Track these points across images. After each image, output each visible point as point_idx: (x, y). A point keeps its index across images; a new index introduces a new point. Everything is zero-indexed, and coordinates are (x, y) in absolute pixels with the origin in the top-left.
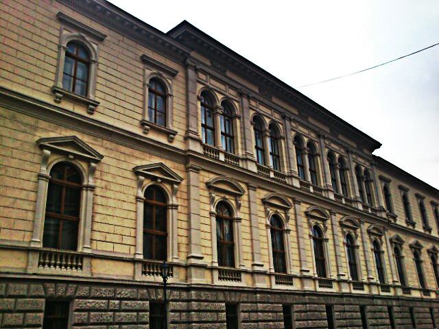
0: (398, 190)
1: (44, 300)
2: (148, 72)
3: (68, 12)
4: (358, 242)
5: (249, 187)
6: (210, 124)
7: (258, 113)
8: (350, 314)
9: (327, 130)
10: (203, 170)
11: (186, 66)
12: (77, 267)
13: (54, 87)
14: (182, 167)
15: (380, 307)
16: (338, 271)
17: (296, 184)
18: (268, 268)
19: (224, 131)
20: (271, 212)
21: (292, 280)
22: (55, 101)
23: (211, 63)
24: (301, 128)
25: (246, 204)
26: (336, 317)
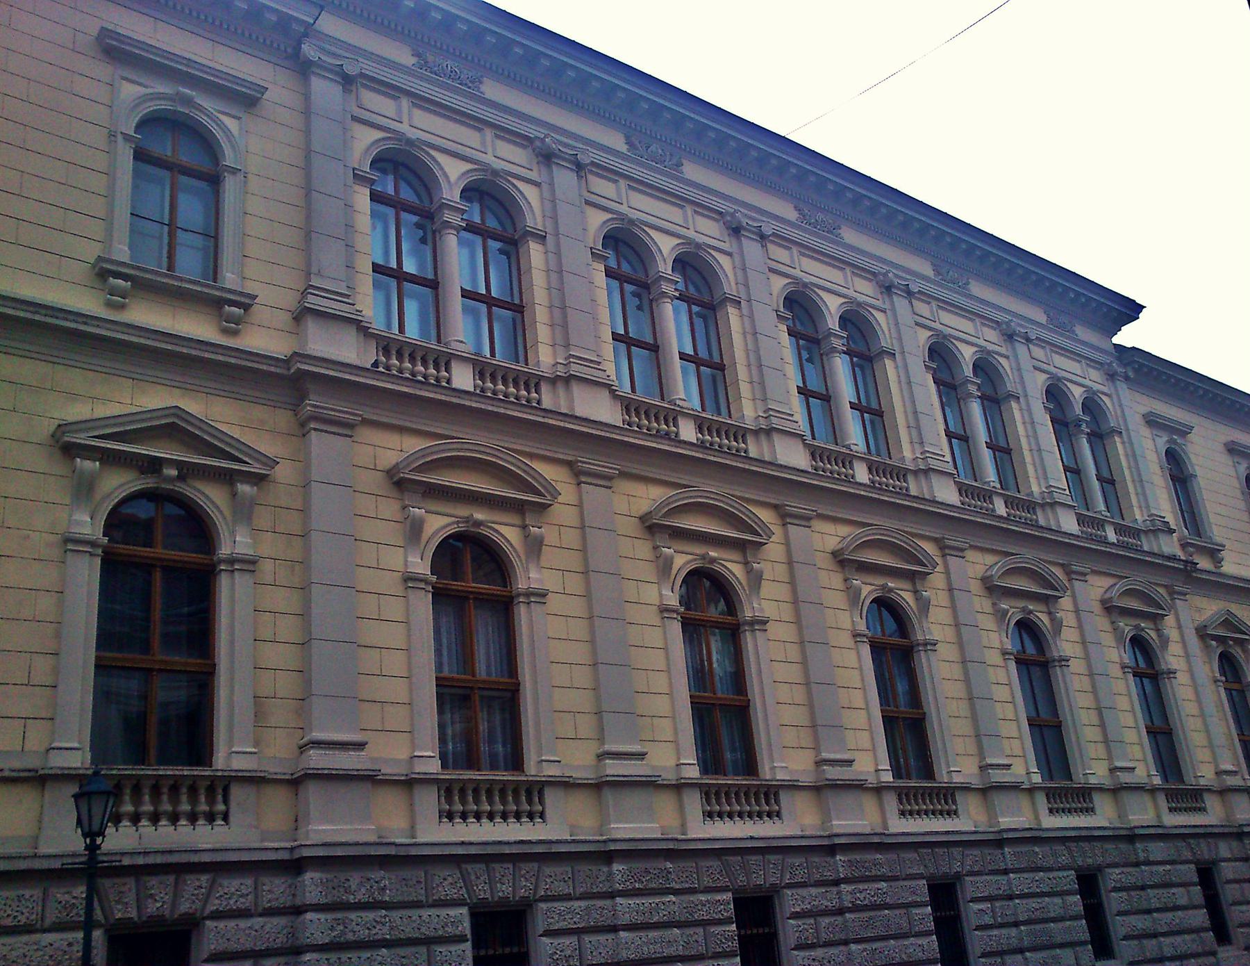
0: (1225, 459)
1: (464, 911)
2: (129, 91)
3: (139, 28)
4: (1066, 644)
5: (785, 517)
6: (814, 384)
7: (938, 333)
8: (1033, 903)
9: (924, 267)
10: (821, 517)
11: (303, 69)
12: (211, 818)
13: (100, 259)
14: (283, 419)
15: (1161, 868)
16: (981, 754)
17: (1069, 523)
18: (1145, 774)
19: (689, 350)
20: (866, 590)
21: (1091, 801)
22: (110, 305)
23: (417, 54)
24: (1060, 361)
25: (781, 571)
26: (974, 921)
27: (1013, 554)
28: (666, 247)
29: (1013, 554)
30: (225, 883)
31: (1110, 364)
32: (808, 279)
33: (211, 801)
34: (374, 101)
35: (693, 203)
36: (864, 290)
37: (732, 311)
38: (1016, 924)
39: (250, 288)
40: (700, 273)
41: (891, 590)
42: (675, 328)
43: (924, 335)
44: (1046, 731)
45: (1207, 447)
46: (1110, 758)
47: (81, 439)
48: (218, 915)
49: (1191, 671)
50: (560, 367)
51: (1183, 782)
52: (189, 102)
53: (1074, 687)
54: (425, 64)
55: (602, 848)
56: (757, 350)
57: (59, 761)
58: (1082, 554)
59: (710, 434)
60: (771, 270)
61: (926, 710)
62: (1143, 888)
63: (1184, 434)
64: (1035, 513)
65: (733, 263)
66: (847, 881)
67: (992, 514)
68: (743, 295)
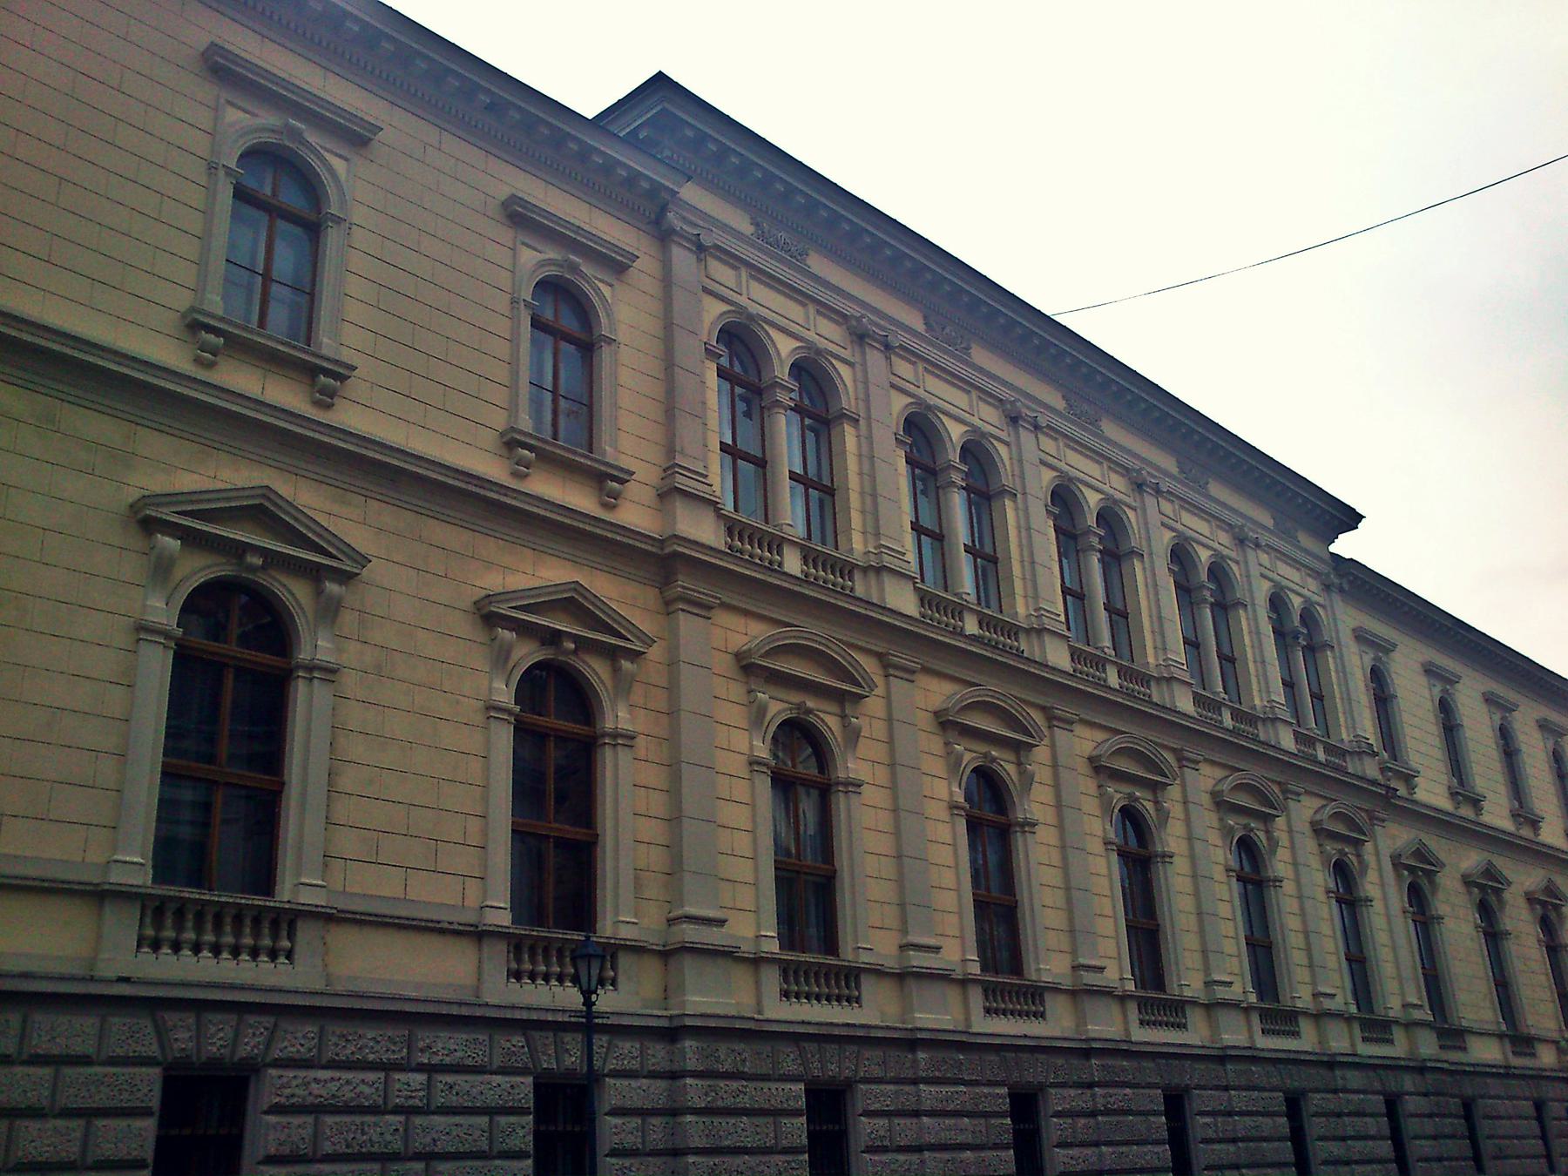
0: (1423, 680)
1: (1004, 1091)
2: (528, 257)
6: (927, 521)
7: (920, 402)
9: (1054, 399)
11: (664, 236)
13: (193, 309)
15: (1355, 1097)
18: (1117, 976)
19: (799, 470)
20: (967, 757)
22: (198, 361)
24: (1187, 518)
26: (1200, 1135)
27: (1239, 770)
28: (784, 348)
29: (1239, 770)
30: (620, 1044)
31: (1328, 575)
32: (754, 309)
33: (275, 936)
34: (722, 273)
35: (1109, 460)
36: (827, 334)
37: (849, 430)
38: (1234, 1141)
39: (346, 356)
40: (817, 383)
41: (809, 711)
42: (787, 443)
43: (1048, 476)
44: (1258, 949)
45: (1408, 665)
46: (1074, 952)
47: (503, 609)
48: (280, 1064)
49: (1385, 898)
50: (872, 557)
51: (1372, 1012)
52: (574, 268)
53: (1175, 883)
54: (762, 235)
55: (909, 1035)
56: (1030, 545)
57: (117, 877)
58: (1195, 738)
59: (741, 539)
60: (893, 386)
61: (286, 778)
62: (1339, 1115)
63: (1387, 651)
64: (1104, 671)
65: (854, 374)
66: (1099, 1084)
67: (959, 633)
68: (1019, 488)
